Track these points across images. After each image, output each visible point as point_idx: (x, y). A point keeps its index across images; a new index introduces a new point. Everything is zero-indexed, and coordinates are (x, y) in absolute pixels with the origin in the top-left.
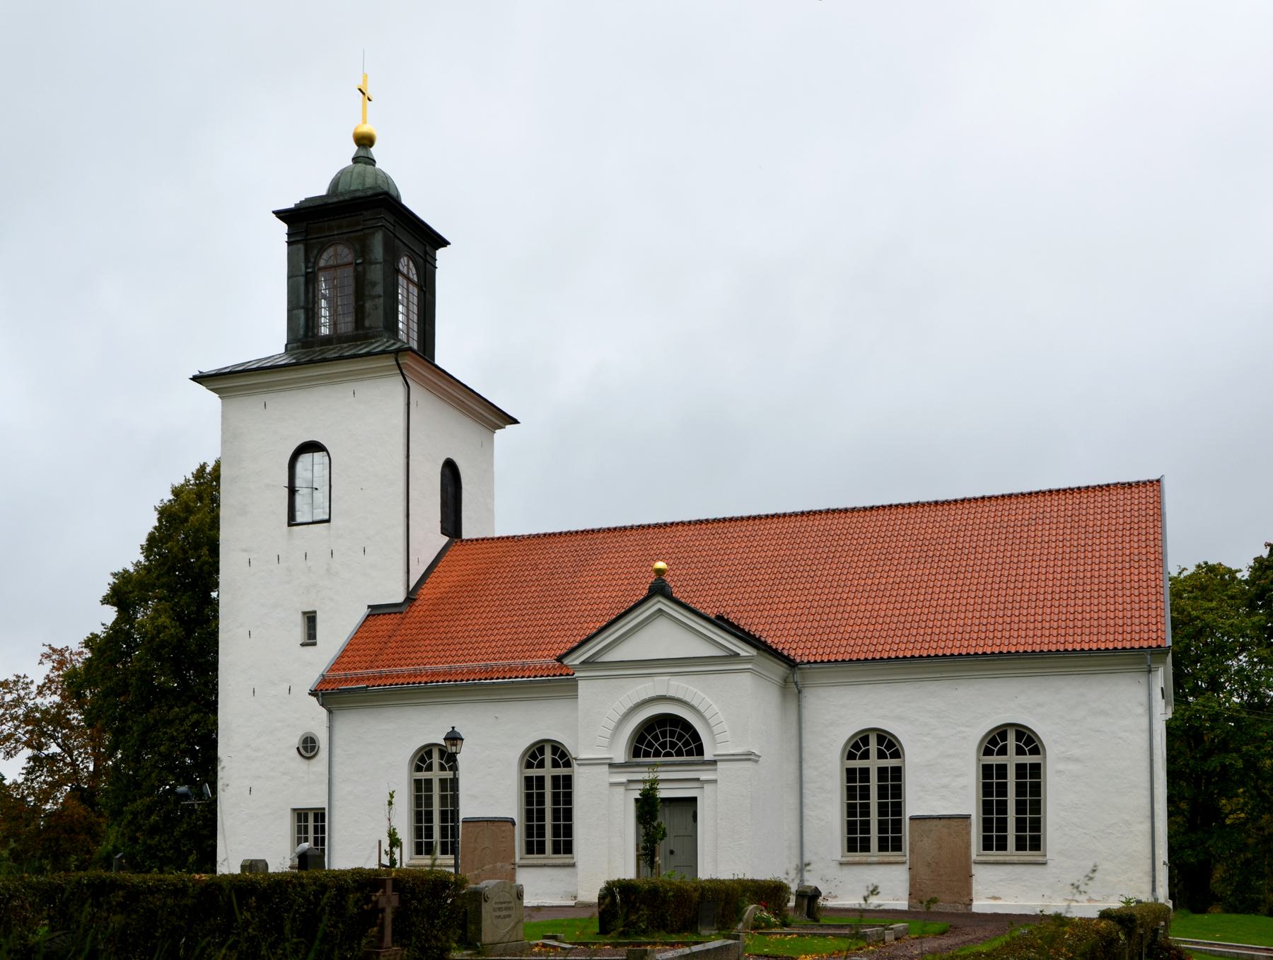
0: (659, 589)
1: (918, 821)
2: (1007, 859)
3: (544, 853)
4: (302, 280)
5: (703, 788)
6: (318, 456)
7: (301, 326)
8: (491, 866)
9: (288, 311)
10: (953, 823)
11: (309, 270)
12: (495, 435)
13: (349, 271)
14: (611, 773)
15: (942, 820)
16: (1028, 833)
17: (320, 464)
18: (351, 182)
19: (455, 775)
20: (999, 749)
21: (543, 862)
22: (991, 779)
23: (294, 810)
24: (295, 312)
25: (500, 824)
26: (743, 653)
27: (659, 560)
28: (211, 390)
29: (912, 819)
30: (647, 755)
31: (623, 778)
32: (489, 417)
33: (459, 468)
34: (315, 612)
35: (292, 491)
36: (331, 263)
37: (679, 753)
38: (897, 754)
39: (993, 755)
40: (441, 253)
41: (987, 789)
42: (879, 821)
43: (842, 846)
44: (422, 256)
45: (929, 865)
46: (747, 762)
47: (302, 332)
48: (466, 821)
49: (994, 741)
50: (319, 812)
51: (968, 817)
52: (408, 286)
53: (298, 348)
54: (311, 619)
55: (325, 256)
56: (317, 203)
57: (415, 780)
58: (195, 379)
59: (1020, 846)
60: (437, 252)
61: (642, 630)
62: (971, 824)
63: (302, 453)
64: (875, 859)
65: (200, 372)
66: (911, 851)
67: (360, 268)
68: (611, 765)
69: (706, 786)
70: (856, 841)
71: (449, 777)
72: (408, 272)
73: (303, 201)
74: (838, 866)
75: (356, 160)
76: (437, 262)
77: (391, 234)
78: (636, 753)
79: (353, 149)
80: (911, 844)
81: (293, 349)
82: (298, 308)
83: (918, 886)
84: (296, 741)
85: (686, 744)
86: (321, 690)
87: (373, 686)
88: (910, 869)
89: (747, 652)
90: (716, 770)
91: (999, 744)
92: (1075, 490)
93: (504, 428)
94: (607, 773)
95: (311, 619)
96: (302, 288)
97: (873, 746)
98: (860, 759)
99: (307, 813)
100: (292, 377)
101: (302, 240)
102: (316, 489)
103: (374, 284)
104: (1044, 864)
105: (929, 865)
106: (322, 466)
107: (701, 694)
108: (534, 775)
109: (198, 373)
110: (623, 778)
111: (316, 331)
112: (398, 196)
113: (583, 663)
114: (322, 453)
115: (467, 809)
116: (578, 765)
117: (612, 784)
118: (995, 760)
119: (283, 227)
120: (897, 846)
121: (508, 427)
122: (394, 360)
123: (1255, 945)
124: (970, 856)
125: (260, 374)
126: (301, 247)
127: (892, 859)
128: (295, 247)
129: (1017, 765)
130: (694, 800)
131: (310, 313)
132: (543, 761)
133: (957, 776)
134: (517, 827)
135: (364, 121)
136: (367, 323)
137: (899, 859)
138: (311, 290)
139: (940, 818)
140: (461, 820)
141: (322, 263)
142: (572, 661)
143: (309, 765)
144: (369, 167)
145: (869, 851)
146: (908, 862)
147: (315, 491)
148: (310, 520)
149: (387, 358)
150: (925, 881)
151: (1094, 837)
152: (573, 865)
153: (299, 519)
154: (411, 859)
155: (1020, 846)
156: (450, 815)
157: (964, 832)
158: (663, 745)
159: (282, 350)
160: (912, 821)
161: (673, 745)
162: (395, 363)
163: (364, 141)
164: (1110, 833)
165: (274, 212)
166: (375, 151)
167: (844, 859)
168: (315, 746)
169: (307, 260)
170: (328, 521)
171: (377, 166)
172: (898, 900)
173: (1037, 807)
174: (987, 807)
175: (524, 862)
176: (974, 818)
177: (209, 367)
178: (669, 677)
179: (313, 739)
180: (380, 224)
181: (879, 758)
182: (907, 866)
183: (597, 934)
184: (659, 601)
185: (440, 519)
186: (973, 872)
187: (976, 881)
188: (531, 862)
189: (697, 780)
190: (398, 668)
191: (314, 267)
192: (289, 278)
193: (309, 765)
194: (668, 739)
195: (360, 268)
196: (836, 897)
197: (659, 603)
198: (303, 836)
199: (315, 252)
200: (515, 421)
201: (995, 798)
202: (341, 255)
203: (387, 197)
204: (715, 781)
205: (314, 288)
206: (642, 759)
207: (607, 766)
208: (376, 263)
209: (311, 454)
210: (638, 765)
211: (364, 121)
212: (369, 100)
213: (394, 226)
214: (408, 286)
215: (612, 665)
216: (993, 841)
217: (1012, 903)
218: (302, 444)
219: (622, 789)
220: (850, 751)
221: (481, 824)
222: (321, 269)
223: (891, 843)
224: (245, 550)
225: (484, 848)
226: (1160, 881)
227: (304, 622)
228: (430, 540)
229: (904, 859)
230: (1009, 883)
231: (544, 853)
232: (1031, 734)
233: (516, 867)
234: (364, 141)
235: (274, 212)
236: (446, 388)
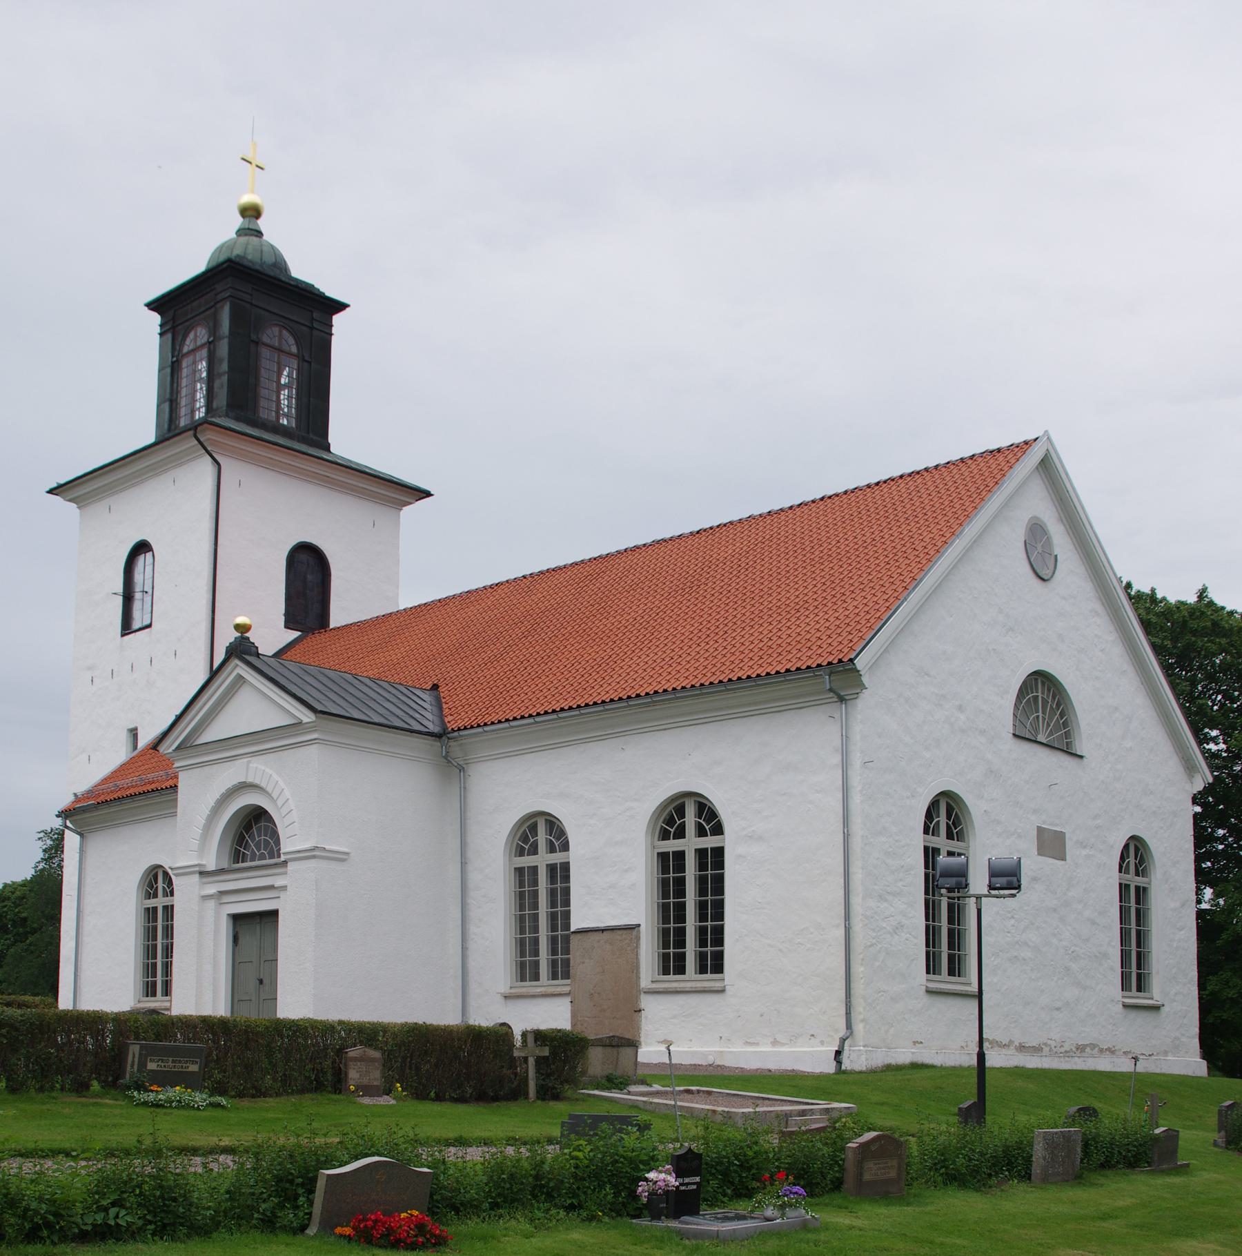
4: (169, 370)
6: (149, 555)
10: (617, 935)
12: (402, 512)
15: (605, 933)
16: (709, 948)
20: (676, 829)
28: (69, 501)
31: (212, 889)
32: (379, 491)
33: (325, 552)
36: (191, 347)
38: (718, 830)
40: (337, 319)
44: (308, 324)
46: (313, 861)
47: (166, 426)
51: (634, 928)
55: (188, 342)
58: (51, 492)
60: (335, 317)
61: (232, 700)
68: (202, 873)
70: (526, 970)
72: (280, 343)
74: (502, 1000)
75: (241, 232)
76: (333, 328)
78: (238, 856)
79: (238, 221)
82: (165, 402)
83: (580, 1026)
90: (285, 873)
96: (169, 379)
97: (690, 819)
100: (119, 477)
101: (169, 330)
103: (221, 361)
104: (722, 991)
110: (212, 889)
112: (280, 265)
113: (178, 748)
119: (156, 318)
126: (169, 336)
131: (174, 405)
132: (682, 826)
133: (626, 871)
138: (176, 381)
144: (254, 240)
152: (147, 996)
153: (136, 625)
157: (629, 948)
162: (196, 442)
163: (251, 212)
164: (799, 943)
166: (262, 223)
170: (149, 626)
171: (265, 237)
176: (643, 928)
185: (284, 612)
186: (643, 1006)
187: (646, 1017)
192: (160, 371)
195: (212, 346)
200: (428, 494)
207: (197, 875)
213: (251, 295)
217: (686, 1049)
218: (137, 543)
219: (211, 904)
223: (561, 970)
224: (89, 668)
226: (860, 1013)
230: (683, 1021)
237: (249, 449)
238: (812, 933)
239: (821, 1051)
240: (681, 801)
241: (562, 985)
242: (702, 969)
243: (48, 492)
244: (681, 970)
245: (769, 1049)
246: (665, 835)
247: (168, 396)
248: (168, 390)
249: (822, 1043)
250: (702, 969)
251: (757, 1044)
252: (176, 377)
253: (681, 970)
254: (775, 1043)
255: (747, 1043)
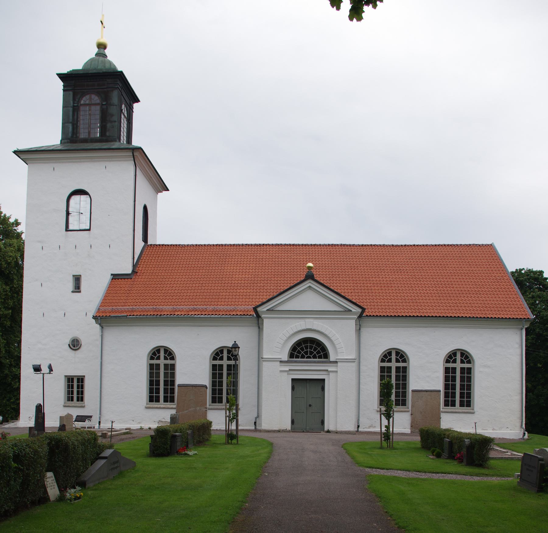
0: (310, 276)
1: (416, 392)
2: (457, 410)
3: (159, 402)
4: (71, 109)
5: (329, 374)
6: (83, 197)
7: (70, 132)
8: (194, 409)
9: (63, 124)
10: (433, 393)
11: (76, 105)
12: (158, 195)
13: (98, 108)
14: (280, 365)
15: (428, 392)
17: (84, 201)
18: (98, 64)
19: (236, 362)
21: (159, 406)
22: (449, 373)
23: (66, 376)
24: (66, 124)
25: (199, 388)
26: (353, 310)
27: (309, 262)
29: (413, 391)
30: (297, 357)
34: (80, 276)
35: (68, 214)
36: (87, 102)
37: (315, 357)
38: (173, 358)
39: (450, 363)
41: (447, 379)
42: (164, 388)
43: (378, 403)
45: (421, 412)
47: (70, 135)
48: (179, 386)
49: (451, 357)
50: (80, 377)
51: (439, 391)
52: (124, 119)
53: (68, 143)
54: (77, 279)
55: (84, 98)
56: (77, 73)
57: (213, 365)
59: (462, 405)
62: (441, 394)
63: (74, 195)
64: (162, 406)
65: (18, 149)
66: (412, 406)
67: (105, 107)
68: (281, 362)
69: (331, 374)
71: (232, 364)
73: (71, 71)
75: (97, 55)
77: (120, 92)
78: (291, 356)
79: (96, 50)
80: (412, 403)
81: (65, 143)
82: (68, 122)
83: (416, 422)
84: (68, 341)
85: (318, 352)
86: (100, 316)
87: (130, 315)
88: (411, 414)
89: (356, 310)
91: (453, 358)
92: (221, 245)
93: (162, 192)
94: (279, 366)
95: (77, 279)
96: (71, 113)
97: (394, 357)
98: (156, 360)
99: (73, 378)
102: (82, 213)
104: (84, 407)
105: (421, 412)
106: (85, 202)
107: (330, 329)
108: (218, 364)
109: (17, 149)
110: (287, 369)
111: (78, 135)
113: (268, 310)
114: (85, 196)
115: (180, 380)
116: (263, 361)
117: (281, 371)
118: (451, 365)
120: (172, 400)
121: (164, 192)
122: (132, 153)
123: (518, 452)
124: (440, 409)
125: (44, 153)
126: (71, 93)
127: (402, 410)
128: (67, 92)
129: (461, 368)
130: (323, 380)
131: (75, 126)
132: (159, 356)
134: (208, 390)
135: (102, 37)
136: (108, 134)
137: (406, 410)
139: (427, 391)
140: (410, 391)
141: (82, 102)
142: (262, 309)
143: (75, 353)
144: (103, 59)
145: (455, 406)
146: (410, 411)
147: (81, 214)
148: (78, 229)
149: (127, 152)
150: (419, 420)
151: (496, 402)
153: (71, 228)
154: (147, 404)
155: (462, 405)
156: (170, 382)
157: (438, 398)
158: (306, 353)
159: (59, 143)
160: (413, 392)
161: (311, 353)
162: (132, 154)
163: (102, 46)
164: (503, 400)
165: (58, 74)
166: (107, 52)
167: (148, 406)
168: (79, 344)
169: (74, 99)
170: (89, 230)
172: (405, 429)
173: (469, 387)
174: (446, 387)
175: (211, 407)
177: (22, 147)
178: (313, 320)
179: (77, 340)
180: (116, 87)
181: (456, 363)
182: (410, 413)
183: (416, 449)
184: (310, 282)
187: (442, 420)
188: (151, 406)
189: (327, 370)
190: (161, 307)
191: (78, 104)
192: (64, 107)
193: (75, 353)
194: (309, 350)
196: (375, 427)
197: (309, 283)
198: (70, 389)
199: (79, 96)
201: (450, 383)
202: (93, 99)
203: (121, 74)
204: (336, 372)
205: (78, 114)
206: (295, 359)
207: (279, 362)
208: (113, 105)
209: (80, 196)
210: (291, 362)
211: (102, 37)
212: (104, 27)
214: (124, 119)
215: (282, 312)
216: (449, 402)
219: (286, 373)
220: (214, 356)
221: (189, 387)
222: (81, 105)
223: (169, 399)
224: (39, 242)
225: (190, 400)
227: (73, 281)
228: (140, 245)
229: (408, 410)
230: (457, 422)
231: (159, 402)
232: (467, 354)
233: (208, 410)
234: (102, 46)
235: (58, 74)
236: (147, 169)
237: (145, 166)
238: (508, 397)
239: (512, 433)
240: (391, 350)
241: (168, 405)
242: (78, 400)
243: (15, 152)
244: (72, 400)
245: (491, 431)
246: (152, 358)
247: (71, 121)
248: (71, 118)
249: (511, 430)
250: (78, 400)
251: (487, 430)
252: (76, 114)
253: (72, 400)
254: (493, 429)
255: (483, 429)
